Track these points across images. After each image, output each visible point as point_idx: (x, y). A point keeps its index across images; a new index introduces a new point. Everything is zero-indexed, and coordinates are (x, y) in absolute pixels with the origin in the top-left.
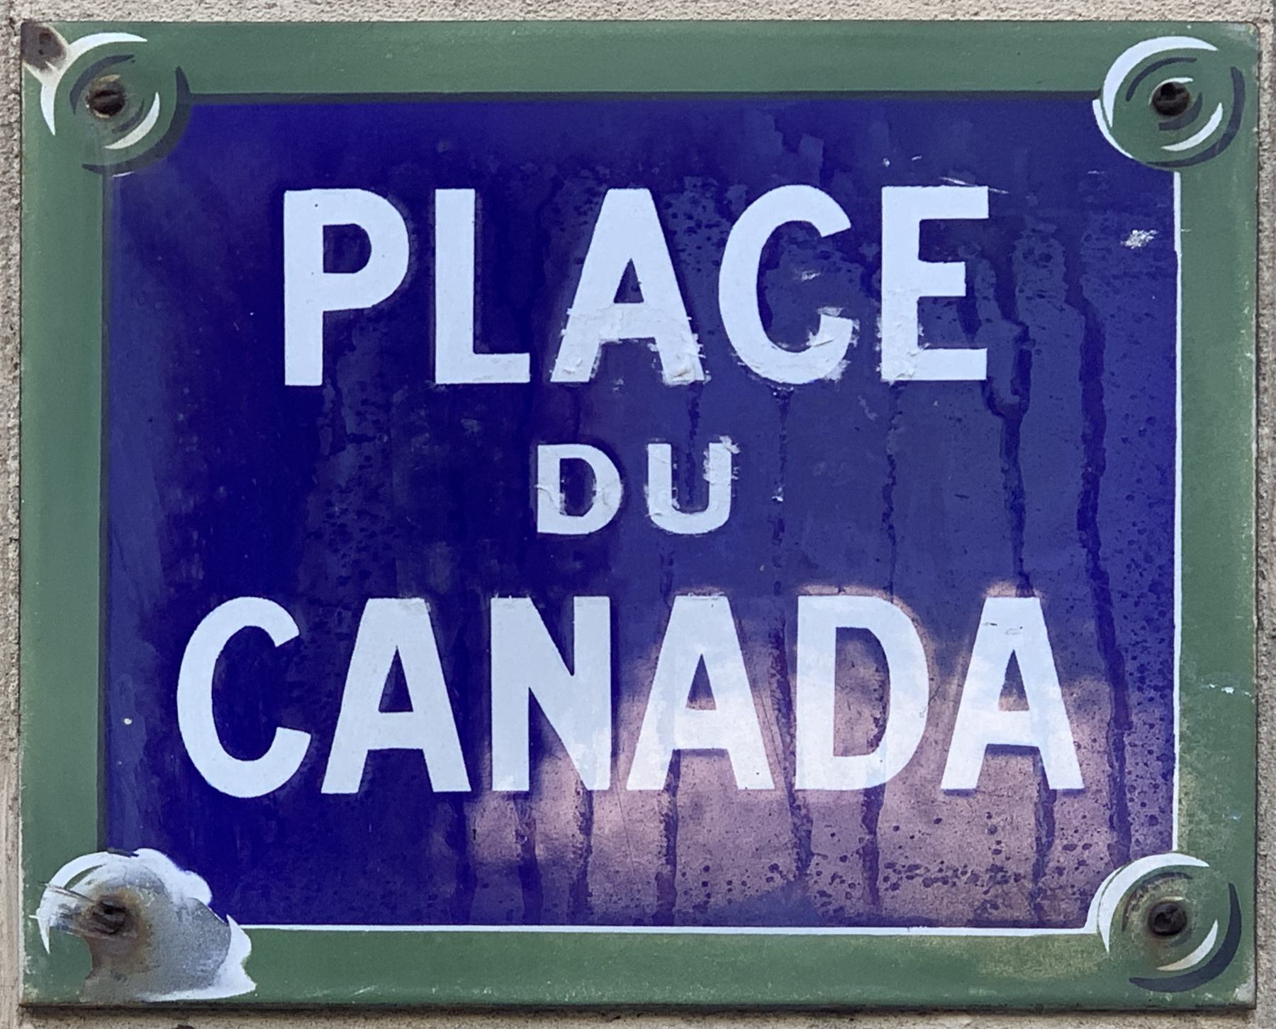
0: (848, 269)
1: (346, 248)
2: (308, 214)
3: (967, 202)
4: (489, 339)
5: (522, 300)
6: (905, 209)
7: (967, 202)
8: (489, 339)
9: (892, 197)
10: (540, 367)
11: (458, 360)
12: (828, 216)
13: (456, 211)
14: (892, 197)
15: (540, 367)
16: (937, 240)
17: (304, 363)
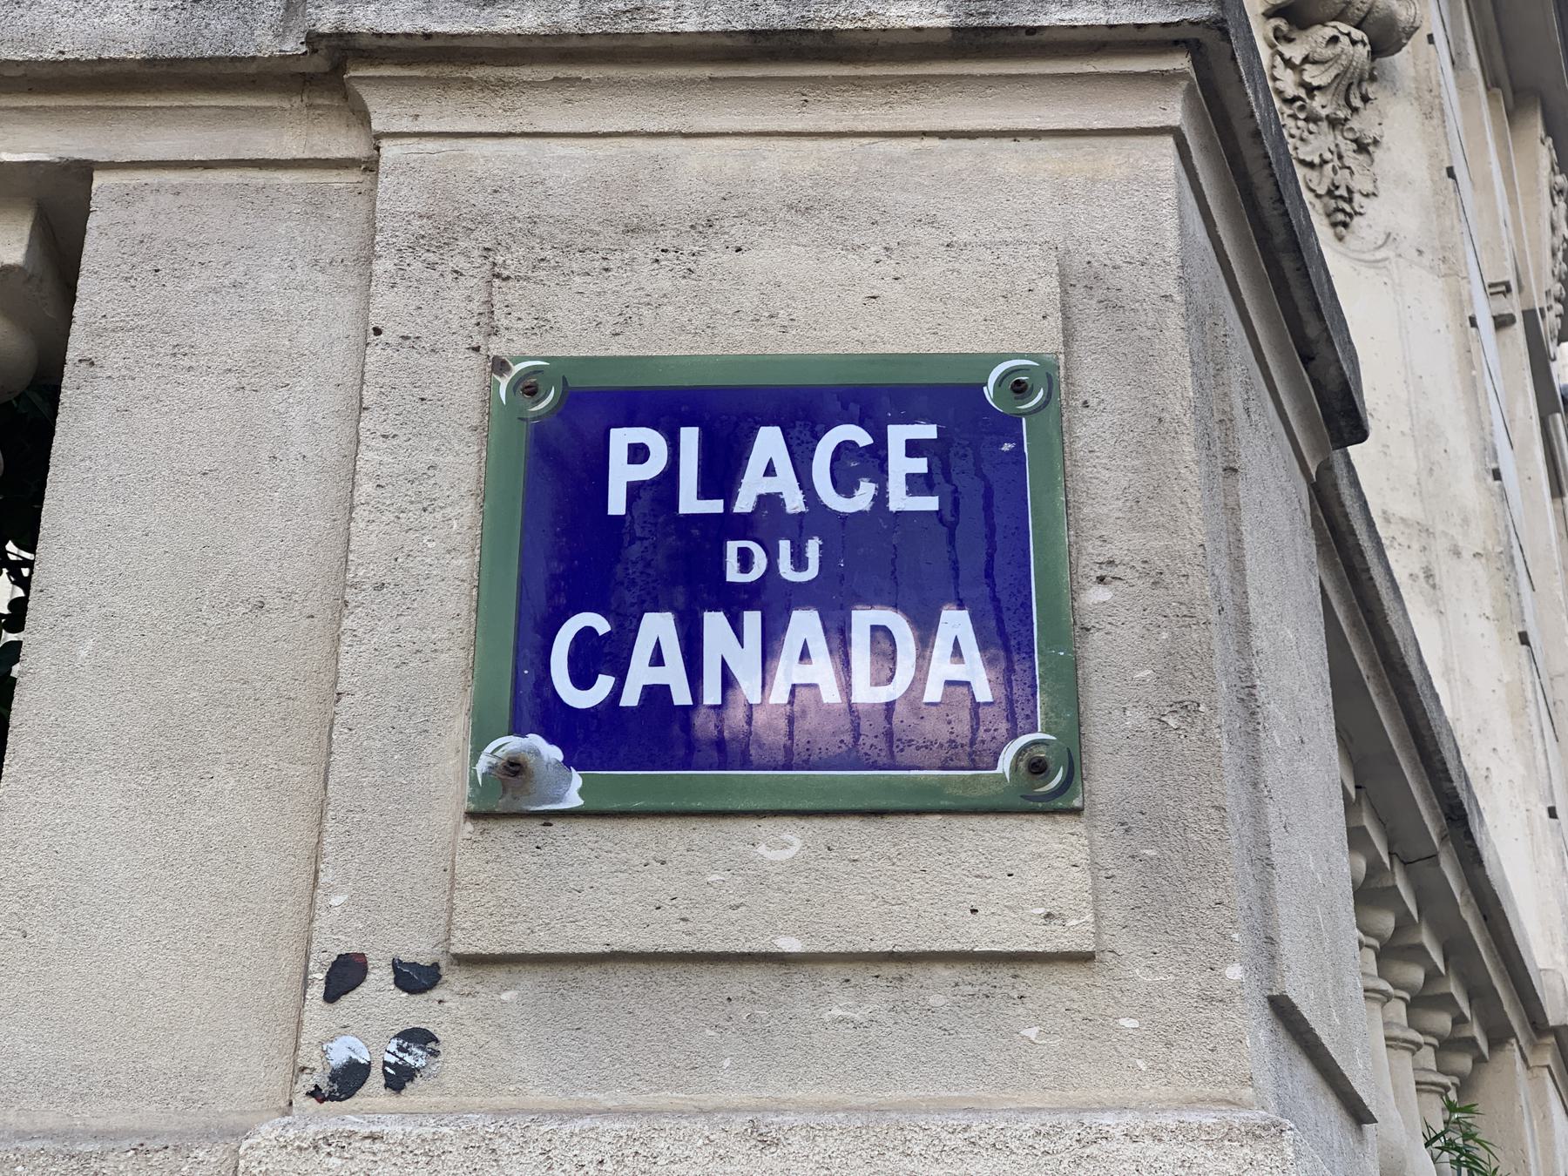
0: (874, 460)
2: (621, 439)
4: (704, 493)
5: (721, 473)
6: (898, 435)
7: (928, 432)
8: (704, 493)
13: (690, 437)
15: (728, 505)
16: (913, 448)
17: (617, 504)
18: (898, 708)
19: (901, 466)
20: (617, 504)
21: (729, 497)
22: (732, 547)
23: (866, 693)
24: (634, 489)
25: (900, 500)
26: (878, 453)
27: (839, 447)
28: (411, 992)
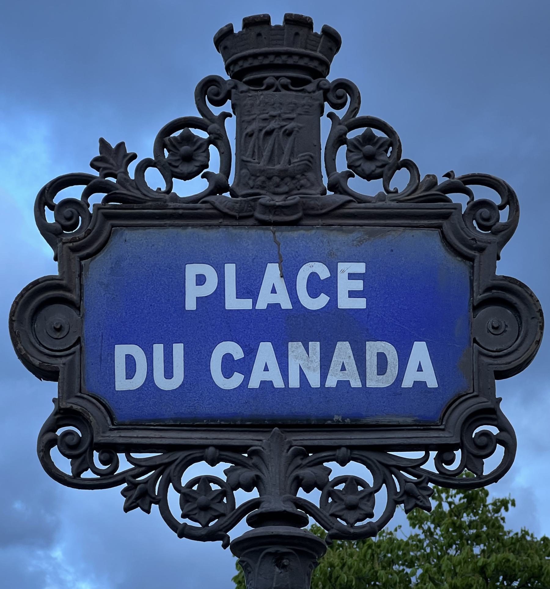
0: (329, 287)
1: (201, 280)
2: (192, 271)
3: (360, 268)
4: (240, 295)
5: (249, 287)
6: (345, 268)
7: (360, 268)
8: (240, 295)
9: (341, 266)
10: (254, 304)
11: (233, 302)
12: (238, 353)
13: (230, 270)
14: (341, 266)
15: (254, 304)
16: (352, 276)
17: (191, 305)
19: (345, 285)
20: (191, 305)
21: (255, 297)
24: (199, 300)
25: (345, 302)
27: (311, 273)
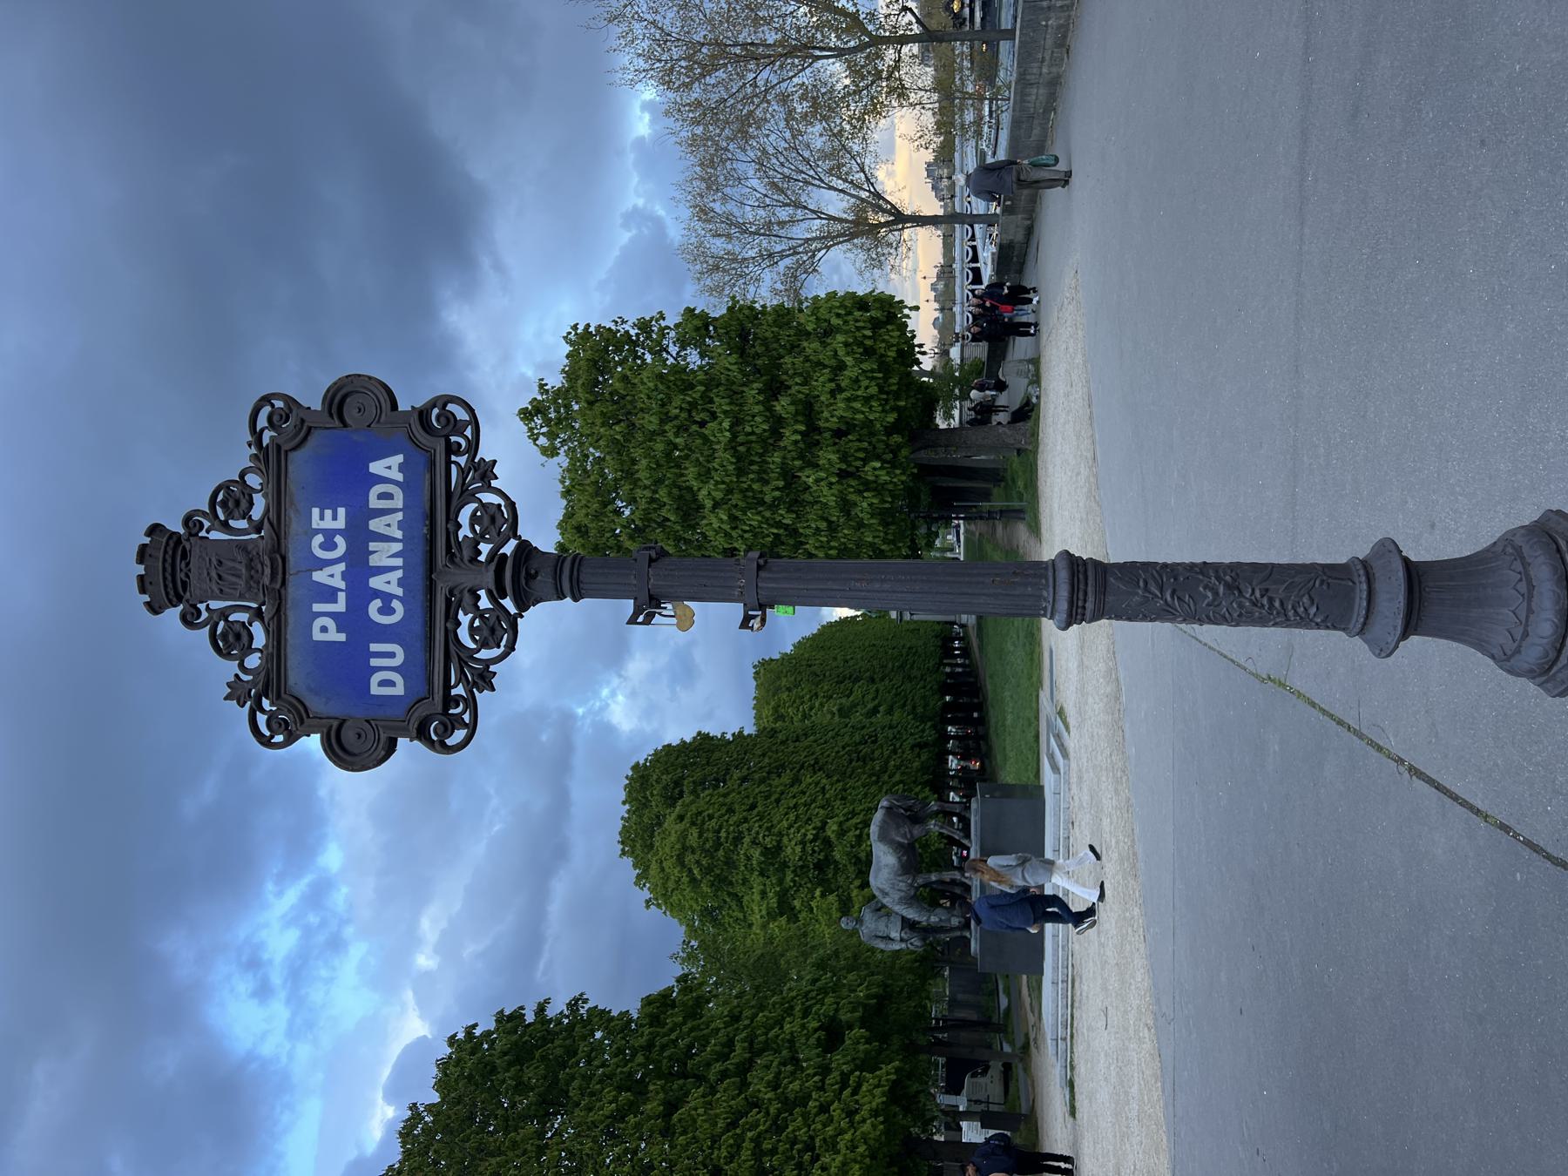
0: (329, 535)
2: (318, 636)
4: (335, 601)
5: (330, 594)
6: (316, 523)
7: (316, 511)
8: (335, 601)
13: (317, 607)
16: (322, 518)
17: (342, 637)
18: (1357, 630)
19: (328, 524)
20: (342, 637)
21: (335, 590)
22: (375, 690)
23: (398, 502)
25: (341, 523)
26: (324, 532)
28: (630, 789)
